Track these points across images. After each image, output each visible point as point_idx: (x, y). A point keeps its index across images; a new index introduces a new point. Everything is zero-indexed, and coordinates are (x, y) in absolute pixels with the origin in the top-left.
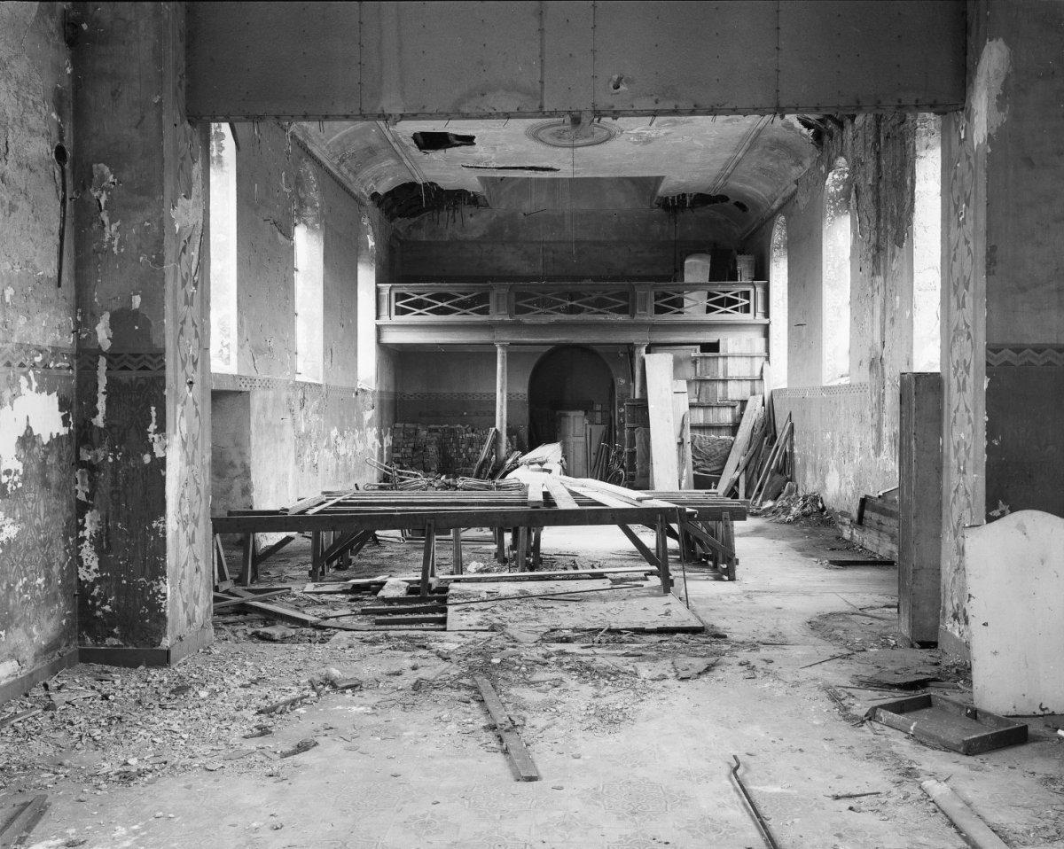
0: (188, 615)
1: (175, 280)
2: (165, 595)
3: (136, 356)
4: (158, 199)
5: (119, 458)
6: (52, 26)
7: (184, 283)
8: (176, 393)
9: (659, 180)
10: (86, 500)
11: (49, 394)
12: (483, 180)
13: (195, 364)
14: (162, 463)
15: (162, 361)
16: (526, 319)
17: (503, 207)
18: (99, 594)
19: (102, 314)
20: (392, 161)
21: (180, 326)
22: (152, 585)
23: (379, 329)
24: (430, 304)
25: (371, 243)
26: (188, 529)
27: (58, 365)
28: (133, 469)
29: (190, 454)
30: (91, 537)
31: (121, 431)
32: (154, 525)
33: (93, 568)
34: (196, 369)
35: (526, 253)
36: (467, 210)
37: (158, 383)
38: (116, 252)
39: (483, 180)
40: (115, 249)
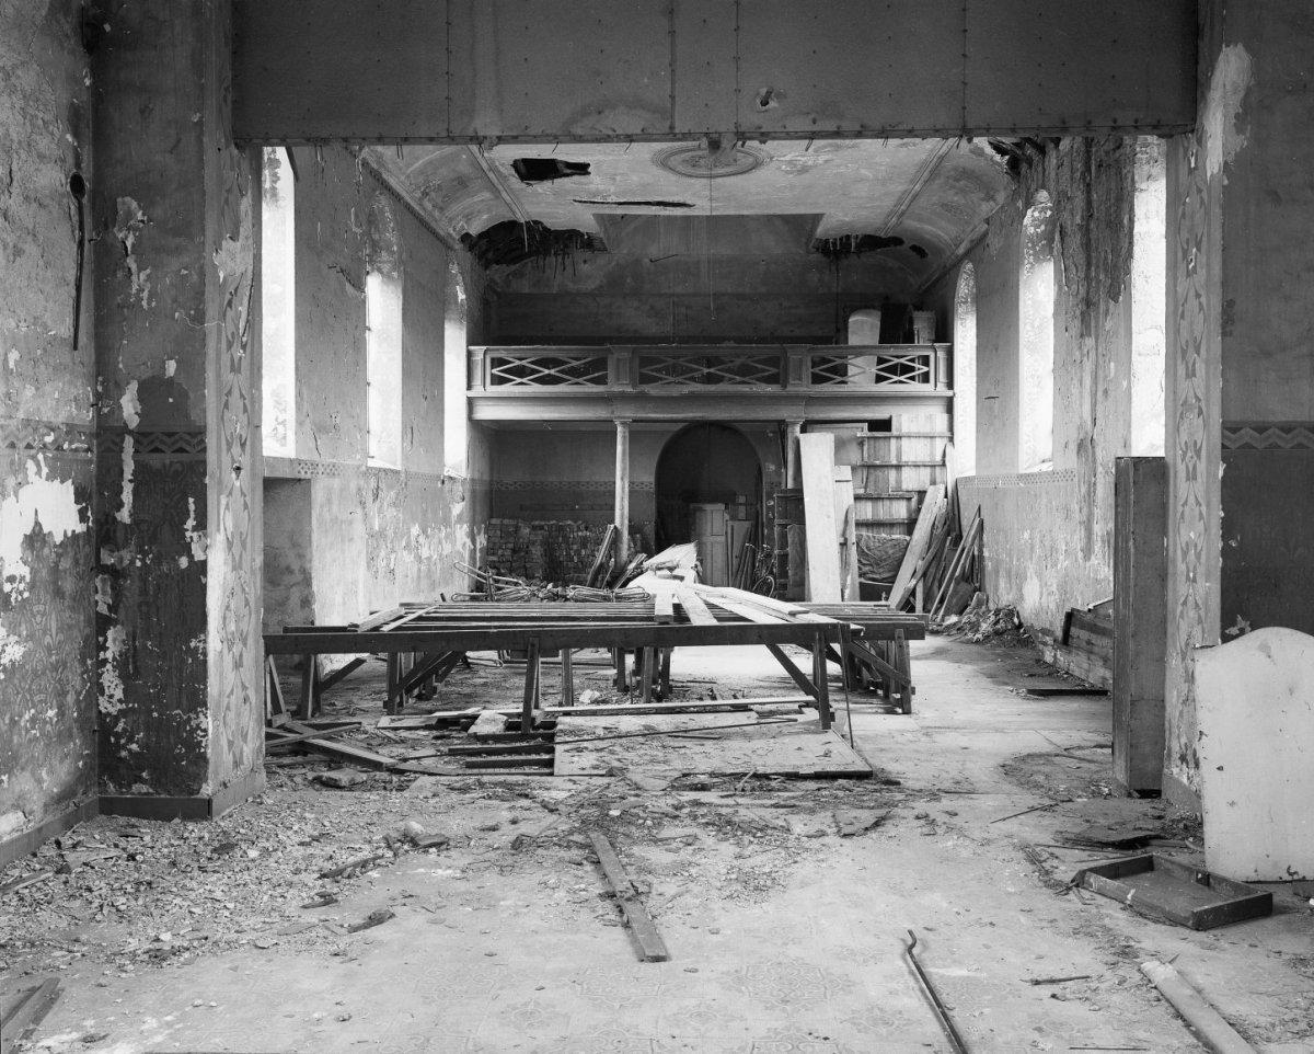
0: (234, 756)
2: (205, 731)
7: (229, 445)
9: (817, 218)
11: (62, 482)
12: (600, 218)
13: (243, 445)
14: (202, 567)
15: (203, 441)
16: (652, 390)
19: (128, 383)
20: (487, 195)
22: (189, 719)
23: (471, 402)
24: (534, 372)
25: (461, 296)
27: (73, 446)
28: (167, 575)
29: (237, 558)
30: (114, 659)
32: (192, 645)
34: (243, 451)
35: (652, 308)
36: (579, 255)
37: (199, 468)
39: (600, 218)
40: (144, 303)
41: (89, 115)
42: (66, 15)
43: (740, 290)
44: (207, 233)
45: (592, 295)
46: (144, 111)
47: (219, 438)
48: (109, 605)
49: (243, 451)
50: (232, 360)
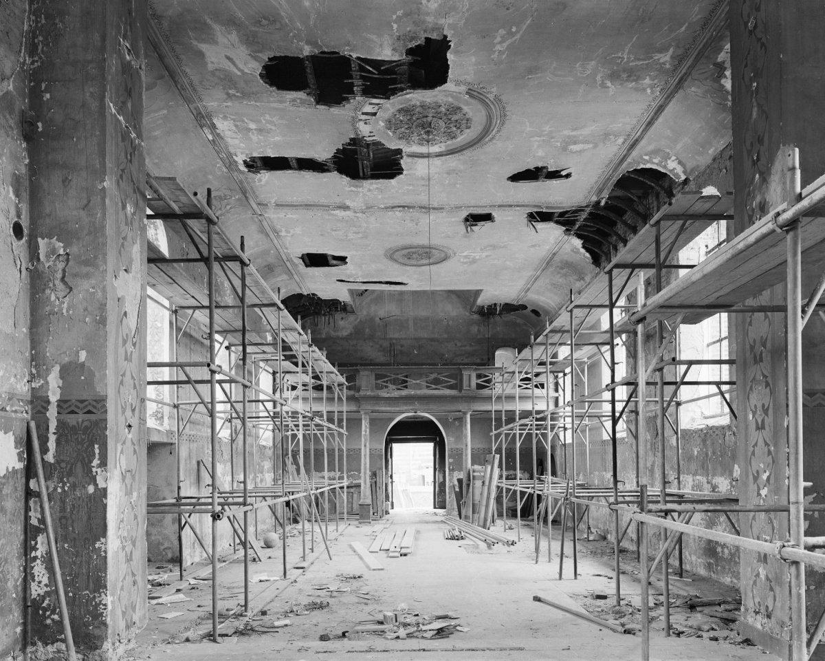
0: (126, 621)
1: (117, 339)
2: (105, 605)
3: (82, 401)
4: (101, 269)
5: (66, 488)
6: (12, 122)
7: (125, 342)
8: (117, 434)
9: (477, 293)
10: (37, 525)
11: (5, 433)
12: (351, 292)
13: (133, 410)
14: (104, 493)
15: (104, 406)
16: (383, 394)
17: (365, 313)
18: (49, 605)
19: (53, 367)
20: (285, 277)
21: (120, 378)
22: (94, 597)
26: (127, 549)
27: (14, 409)
28: (79, 498)
29: (129, 486)
30: (42, 556)
31: (69, 466)
32: (97, 546)
33: (43, 583)
34: (134, 414)
35: (381, 346)
36: (338, 316)
37: (101, 424)
38: (65, 314)
39: (351, 292)
40: (64, 311)
41: (27, 183)
42: (10, 114)
43: (432, 336)
44: (108, 264)
45: (346, 339)
46: (65, 181)
47: (117, 339)
48: (38, 519)
49: (134, 414)
50: (126, 352)
